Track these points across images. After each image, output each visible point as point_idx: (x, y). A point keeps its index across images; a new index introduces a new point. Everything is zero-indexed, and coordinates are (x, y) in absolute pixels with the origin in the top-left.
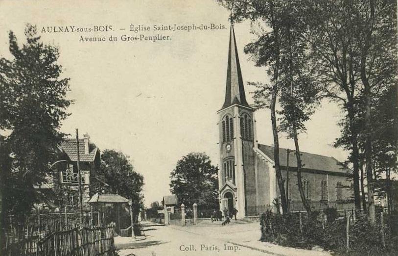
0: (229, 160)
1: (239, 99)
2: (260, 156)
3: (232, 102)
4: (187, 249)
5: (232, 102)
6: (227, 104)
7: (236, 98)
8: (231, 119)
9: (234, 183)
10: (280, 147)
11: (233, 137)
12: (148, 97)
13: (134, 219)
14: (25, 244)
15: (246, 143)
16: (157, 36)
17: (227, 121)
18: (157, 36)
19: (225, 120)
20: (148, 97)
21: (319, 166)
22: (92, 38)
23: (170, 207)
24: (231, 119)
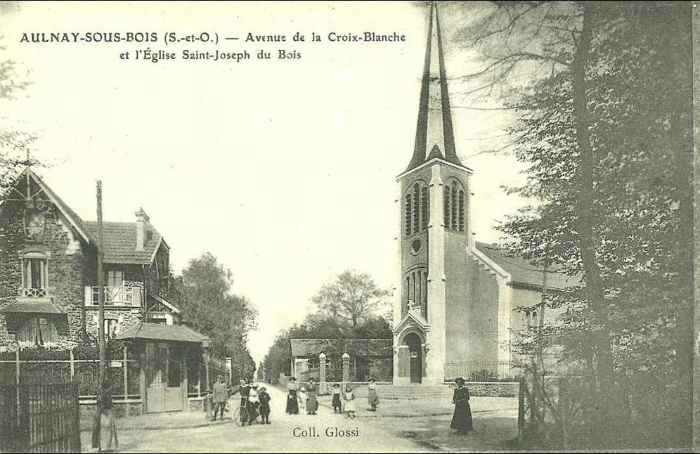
0: (417, 270)
1: (442, 148)
2: (481, 263)
3: (427, 156)
4: (304, 434)
5: (427, 156)
6: (419, 157)
7: (435, 147)
8: (425, 189)
9: (425, 315)
10: (103, 220)
11: (427, 224)
12: (42, 131)
13: (130, 385)
14: (21, 424)
15: (456, 237)
16: (348, 36)
17: (417, 195)
18: (348, 36)
19: (411, 191)
20: (42, 131)
21: (432, 272)
22: (191, 36)
23: (300, 360)
24: (425, 189)
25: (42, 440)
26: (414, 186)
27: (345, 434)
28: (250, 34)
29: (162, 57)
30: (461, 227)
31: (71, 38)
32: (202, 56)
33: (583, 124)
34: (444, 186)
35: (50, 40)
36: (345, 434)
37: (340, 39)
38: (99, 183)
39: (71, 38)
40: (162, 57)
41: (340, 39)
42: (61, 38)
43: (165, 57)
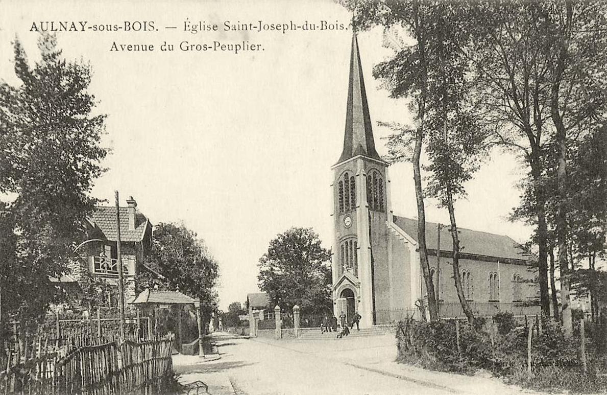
3: (354, 152)
15: (376, 216)
19: (342, 179)
25: (167, 356)
26: (345, 175)
27: (270, 27)
28: (34, 23)
29: (202, 28)
30: (382, 207)
31: (79, 27)
32: (144, 48)
33: (559, 155)
34: (367, 176)
35: (59, 30)
36: (270, 27)
37: (194, 48)
38: (117, 193)
39: (79, 27)
40: (202, 28)
41: (194, 48)
42: (69, 26)
43: (206, 28)
